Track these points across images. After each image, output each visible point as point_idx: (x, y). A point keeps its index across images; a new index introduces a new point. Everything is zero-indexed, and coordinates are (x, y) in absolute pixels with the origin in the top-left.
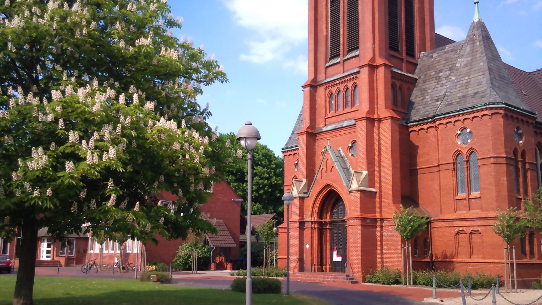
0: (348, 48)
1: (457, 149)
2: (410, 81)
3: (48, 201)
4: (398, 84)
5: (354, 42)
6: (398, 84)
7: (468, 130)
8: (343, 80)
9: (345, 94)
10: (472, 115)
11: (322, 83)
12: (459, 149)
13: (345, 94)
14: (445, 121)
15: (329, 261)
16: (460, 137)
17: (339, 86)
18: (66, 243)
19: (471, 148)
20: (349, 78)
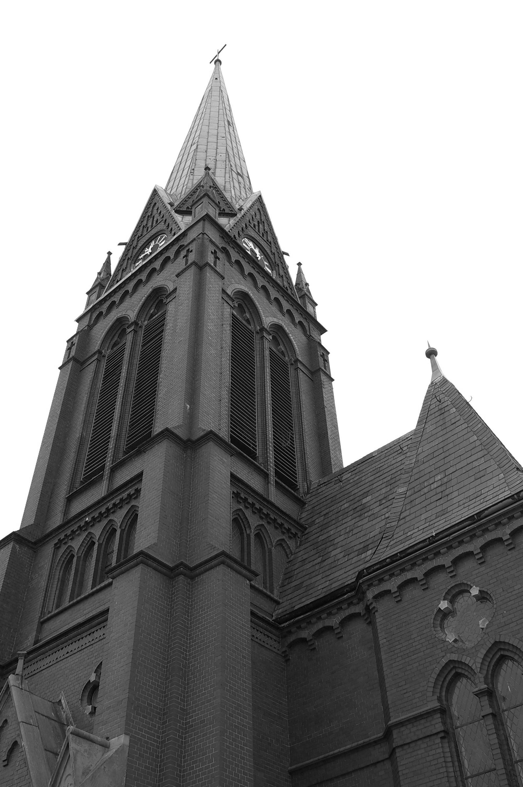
0: (127, 445)
1: (444, 661)
2: (286, 526)
3: (448, 719)
4: (254, 521)
5: (111, 367)
6: (254, 521)
7: (475, 591)
8: (103, 510)
9: (103, 546)
10: (480, 542)
11: (50, 529)
12: (454, 657)
13: (103, 546)
14: (392, 585)
15: (416, 561)
16: (450, 621)
17: (92, 531)
18: (269, 762)
19: (496, 643)
20: (117, 500)
